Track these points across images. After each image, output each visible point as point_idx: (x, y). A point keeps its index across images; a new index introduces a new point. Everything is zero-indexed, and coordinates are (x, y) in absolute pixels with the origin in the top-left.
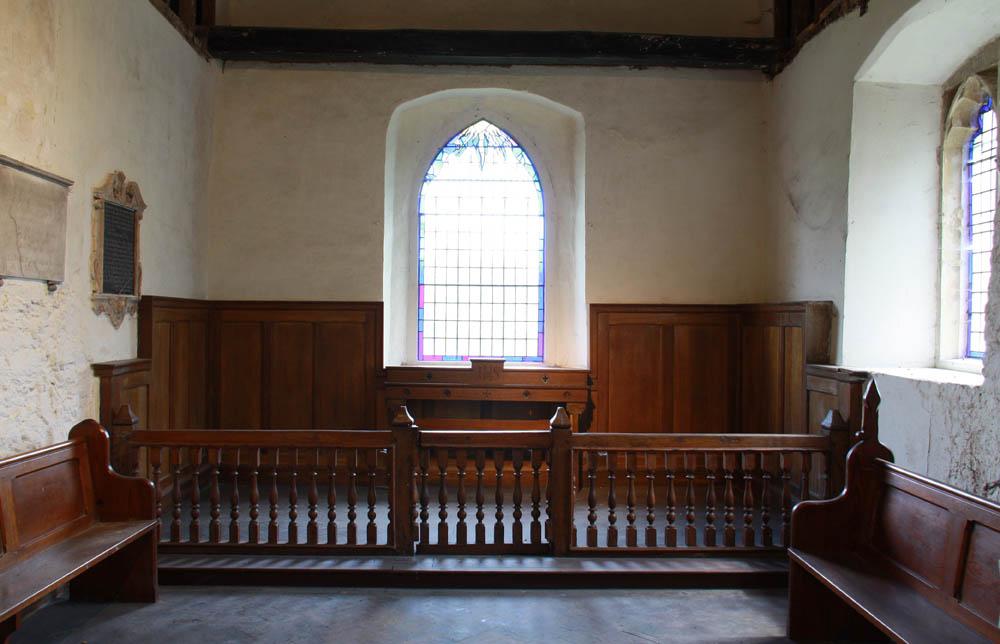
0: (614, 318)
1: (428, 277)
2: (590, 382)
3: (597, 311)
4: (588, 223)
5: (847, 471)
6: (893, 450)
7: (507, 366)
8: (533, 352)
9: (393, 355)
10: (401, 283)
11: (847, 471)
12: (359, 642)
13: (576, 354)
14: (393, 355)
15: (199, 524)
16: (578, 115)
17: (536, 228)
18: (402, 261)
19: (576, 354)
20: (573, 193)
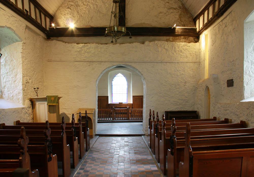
0: (135, 97)
1: (113, 93)
2: (133, 105)
3: (133, 96)
4: (132, 86)
5: (228, 144)
6: (90, 117)
7: (123, 103)
8: (126, 102)
9: (109, 102)
10: (110, 94)
11: (228, 144)
12: (253, 106)
13: (131, 102)
14: (109, 102)
15: (55, 114)
16: (131, 73)
17: (126, 87)
18: (110, 91)
19: (131, 102)
20: (131, 82)
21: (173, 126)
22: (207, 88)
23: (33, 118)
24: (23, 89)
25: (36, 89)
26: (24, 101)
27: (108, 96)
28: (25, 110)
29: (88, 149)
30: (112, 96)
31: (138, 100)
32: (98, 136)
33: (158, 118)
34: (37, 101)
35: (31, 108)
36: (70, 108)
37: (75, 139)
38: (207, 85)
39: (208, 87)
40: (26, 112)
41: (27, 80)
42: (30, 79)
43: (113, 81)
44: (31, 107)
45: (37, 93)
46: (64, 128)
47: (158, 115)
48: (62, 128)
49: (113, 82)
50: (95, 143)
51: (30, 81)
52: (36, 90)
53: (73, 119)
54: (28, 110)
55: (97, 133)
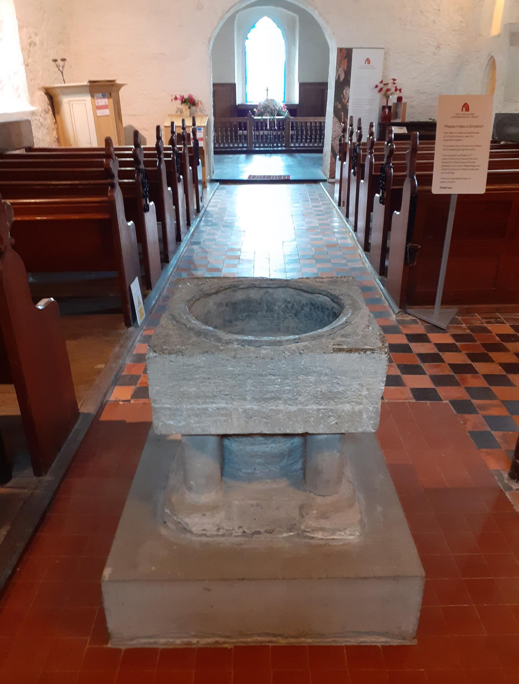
9: (239, 101)
14: (239, 101)
20: (294, 44)
21: (388, 143)
22: (492, 63)
23: (58, 139)
24: (26, 63)
25: (60, 62)
26: (31, 93)
27: (236, 82)
28: (37, 118)
29: (200, 208)
30: (246, 84)
31: (313, 95)
32: (218, 183)
33: (361, 132)
34: (64, 94)
35: (51, 112)
36: (150, 113)
37: (148, 206)
38: (492, 54)
39: (494, 60)
40: (42, 124)
41: (30, 37)
42: (36, 35)
43: (247, 39)
44: (49, 110)
45: (62, 73)
46: (116, 174)
47: (360, 124)
48: (108, 174)
49: (247, 43)
50: (212, 197)
51: (37, 40)
52: (59, 63)
53: (159, 138)
54: (45, 119)
55: (214, 177)
